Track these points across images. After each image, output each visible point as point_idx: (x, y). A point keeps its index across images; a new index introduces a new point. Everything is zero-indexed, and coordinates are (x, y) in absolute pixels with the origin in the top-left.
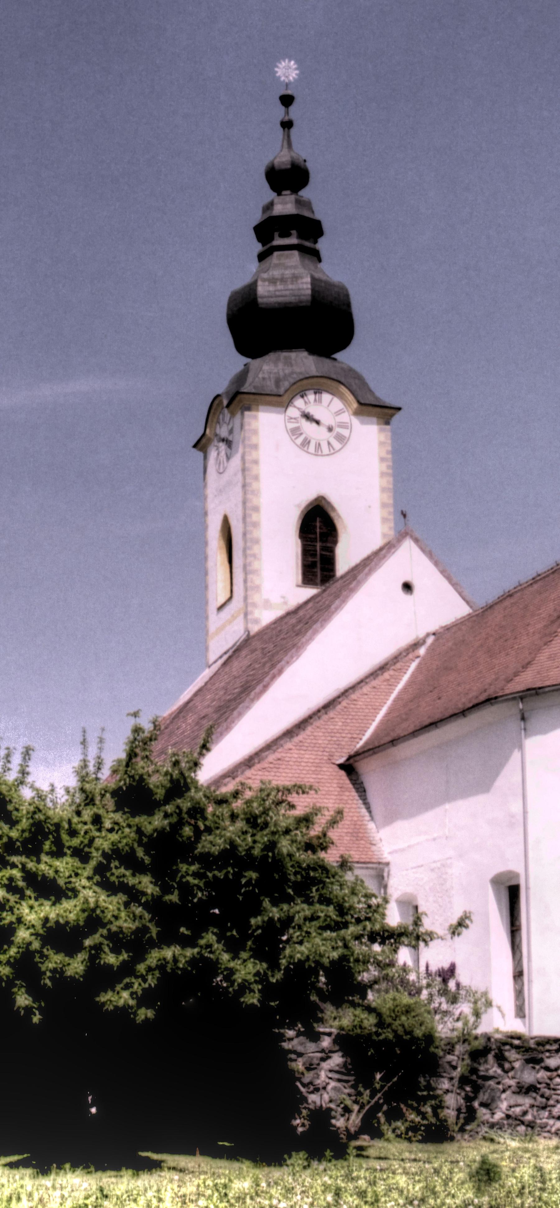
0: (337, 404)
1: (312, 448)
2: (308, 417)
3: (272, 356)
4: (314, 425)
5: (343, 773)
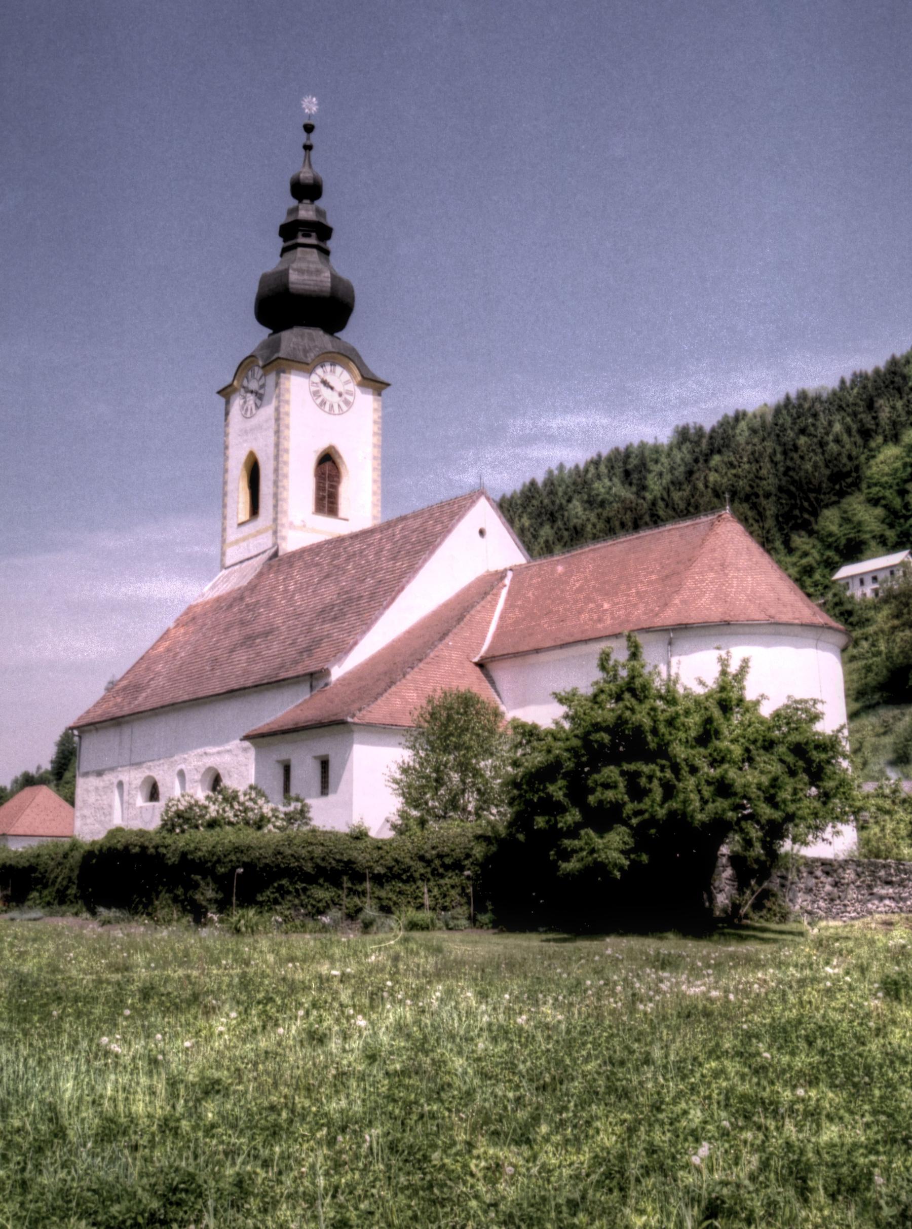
0: (346, 376)
1: (327, 408)
2: (325, 383)
3: (296, 330)
4: (329, 390)
5: (477, 669)
